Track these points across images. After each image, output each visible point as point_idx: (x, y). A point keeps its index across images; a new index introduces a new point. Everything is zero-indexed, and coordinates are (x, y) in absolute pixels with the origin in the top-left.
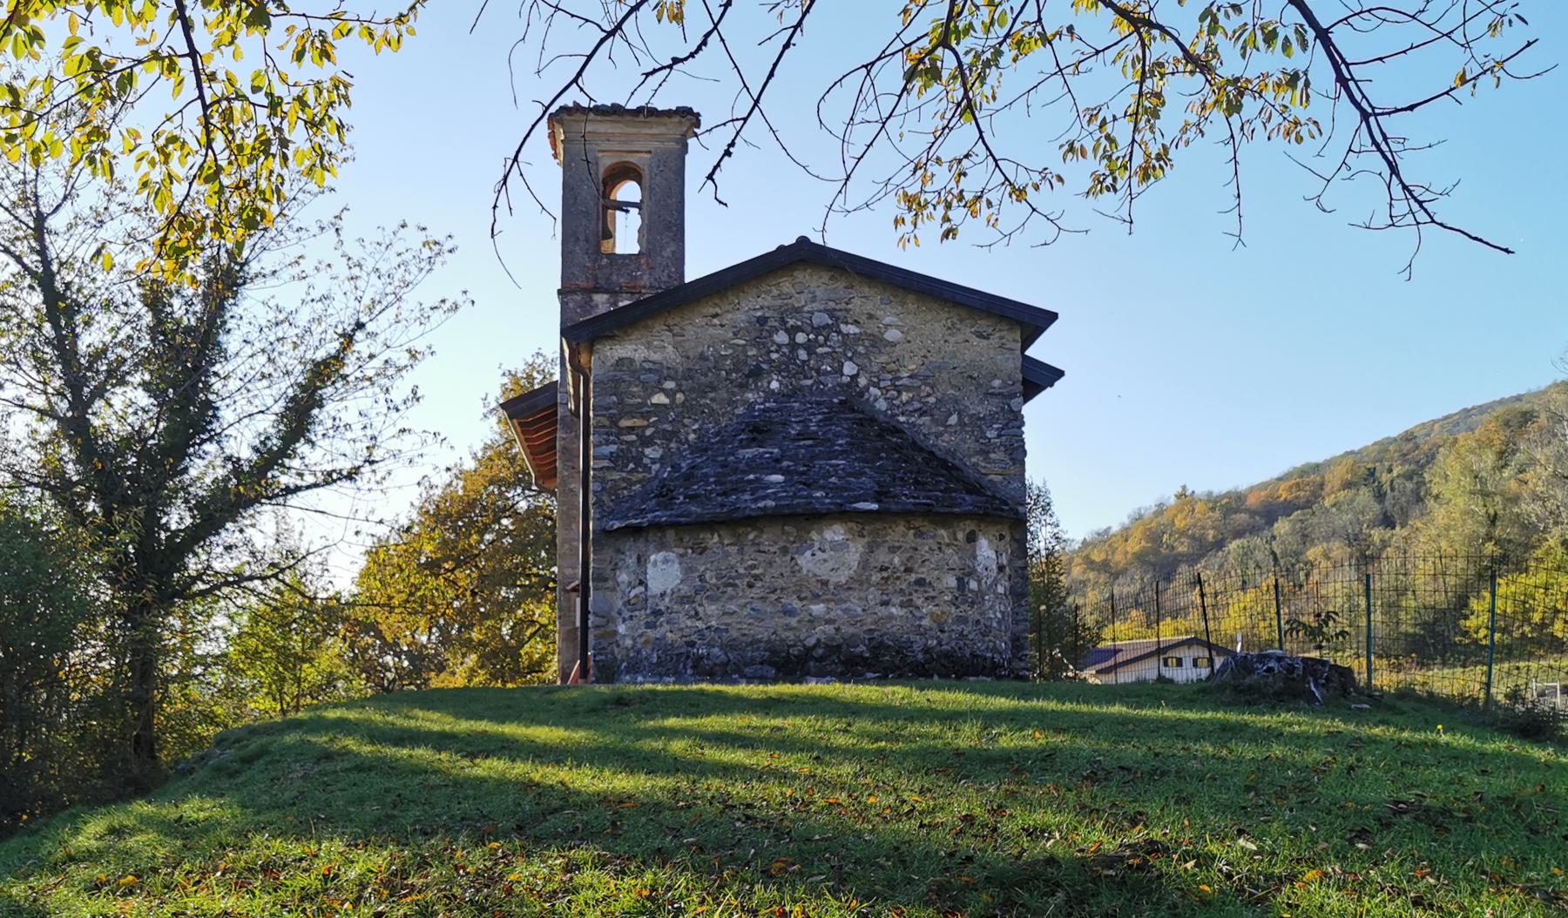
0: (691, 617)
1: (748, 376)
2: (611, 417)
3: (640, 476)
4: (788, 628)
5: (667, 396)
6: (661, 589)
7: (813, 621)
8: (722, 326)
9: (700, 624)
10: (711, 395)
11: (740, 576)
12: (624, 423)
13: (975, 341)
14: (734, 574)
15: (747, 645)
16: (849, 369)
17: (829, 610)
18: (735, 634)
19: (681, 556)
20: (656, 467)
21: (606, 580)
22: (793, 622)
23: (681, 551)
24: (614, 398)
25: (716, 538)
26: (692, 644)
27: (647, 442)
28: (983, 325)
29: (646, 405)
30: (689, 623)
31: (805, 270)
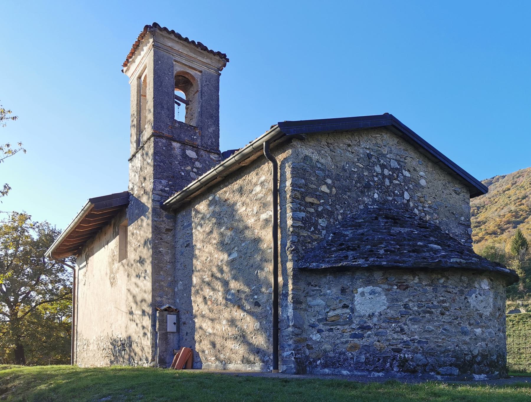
0: (397, 332)
1: (364, 187)
2: (301, 193)
3: (317, 236)
4: (466, 343)
5: (328, 187)
6: (370, 312)
7: (476, 339)
8: (353, 153)
9: (405, 338)
10: (348, 194)
11: (435, 307)
12: (309, 199)
13: (454, 195)
14: (430, 305)
15: (441, 353)
16: (407, 196)
17: (483, 332)
18: (433, 345)
19: (388, 290)
20: (324, 232)
21: (301, 303)
22: (467, 338)
23: (386, 287)
24: (303, 181)
25: (417, 280)
26: (399, 351)
27: (320, 215)
28: (457, 187)
29: (318, 190)
30: (395, 336)
31: (387, 133)
